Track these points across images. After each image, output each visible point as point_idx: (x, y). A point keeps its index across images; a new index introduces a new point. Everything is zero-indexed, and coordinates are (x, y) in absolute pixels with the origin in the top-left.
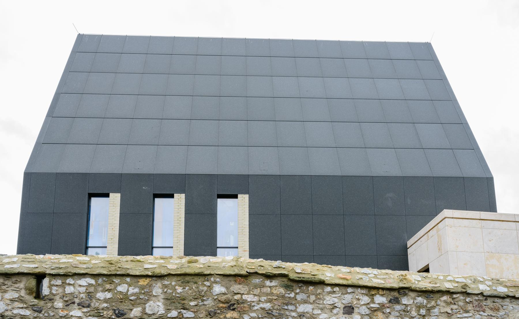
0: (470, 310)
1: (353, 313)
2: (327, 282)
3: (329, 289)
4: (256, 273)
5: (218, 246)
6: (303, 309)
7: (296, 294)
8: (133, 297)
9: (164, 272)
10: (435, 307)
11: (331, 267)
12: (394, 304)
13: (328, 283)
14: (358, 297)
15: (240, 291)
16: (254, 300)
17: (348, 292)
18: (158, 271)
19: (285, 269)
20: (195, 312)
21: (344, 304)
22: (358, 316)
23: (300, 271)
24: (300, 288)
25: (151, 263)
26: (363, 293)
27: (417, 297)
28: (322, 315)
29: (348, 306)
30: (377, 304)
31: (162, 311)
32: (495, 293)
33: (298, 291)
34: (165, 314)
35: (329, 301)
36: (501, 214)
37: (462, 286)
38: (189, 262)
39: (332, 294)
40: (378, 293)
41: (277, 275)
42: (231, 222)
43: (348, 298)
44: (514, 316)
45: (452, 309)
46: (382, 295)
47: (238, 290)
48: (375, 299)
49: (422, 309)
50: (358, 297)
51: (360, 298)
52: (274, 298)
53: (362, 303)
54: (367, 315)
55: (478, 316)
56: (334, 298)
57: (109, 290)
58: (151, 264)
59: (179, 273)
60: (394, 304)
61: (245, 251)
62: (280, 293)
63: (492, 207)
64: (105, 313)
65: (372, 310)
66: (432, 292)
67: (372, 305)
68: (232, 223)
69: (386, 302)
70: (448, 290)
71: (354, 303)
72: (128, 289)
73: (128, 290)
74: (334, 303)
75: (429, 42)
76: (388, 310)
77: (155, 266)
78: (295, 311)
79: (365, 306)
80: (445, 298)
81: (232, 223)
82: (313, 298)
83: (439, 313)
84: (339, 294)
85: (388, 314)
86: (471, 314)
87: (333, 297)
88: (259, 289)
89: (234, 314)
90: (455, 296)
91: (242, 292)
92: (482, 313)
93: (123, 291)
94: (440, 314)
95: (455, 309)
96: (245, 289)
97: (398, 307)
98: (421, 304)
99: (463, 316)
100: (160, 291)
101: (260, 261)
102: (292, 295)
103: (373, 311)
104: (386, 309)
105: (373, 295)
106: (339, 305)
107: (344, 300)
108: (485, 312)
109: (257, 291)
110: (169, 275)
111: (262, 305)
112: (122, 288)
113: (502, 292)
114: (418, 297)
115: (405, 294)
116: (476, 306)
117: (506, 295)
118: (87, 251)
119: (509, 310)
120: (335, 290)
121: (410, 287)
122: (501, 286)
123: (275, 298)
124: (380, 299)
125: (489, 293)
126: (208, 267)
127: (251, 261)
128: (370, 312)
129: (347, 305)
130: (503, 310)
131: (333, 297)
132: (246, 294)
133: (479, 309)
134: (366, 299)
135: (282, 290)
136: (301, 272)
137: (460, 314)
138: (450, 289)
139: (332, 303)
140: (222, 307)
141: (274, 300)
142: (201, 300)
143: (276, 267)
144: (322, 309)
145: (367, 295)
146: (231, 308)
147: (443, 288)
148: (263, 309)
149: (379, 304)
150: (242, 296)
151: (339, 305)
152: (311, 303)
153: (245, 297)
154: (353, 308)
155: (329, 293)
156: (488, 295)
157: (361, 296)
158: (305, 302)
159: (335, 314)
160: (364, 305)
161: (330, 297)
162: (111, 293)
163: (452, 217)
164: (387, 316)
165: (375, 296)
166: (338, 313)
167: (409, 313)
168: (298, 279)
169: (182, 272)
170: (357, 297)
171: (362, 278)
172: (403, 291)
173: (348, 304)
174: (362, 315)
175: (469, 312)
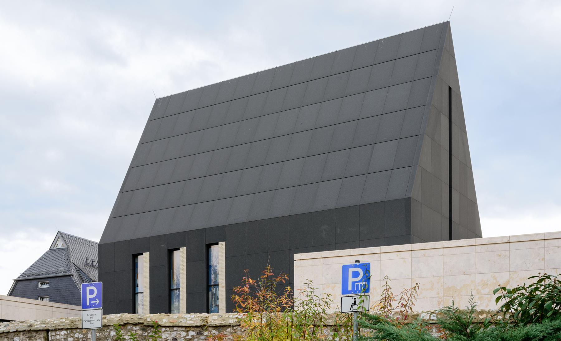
3: (164, 329)
46: (193, 331)
53: (182, 336)
61: (223, 287)
67: (187, 337)
71: (178, 337)
73: (79, 336)
75: (447, 20)
80: (229, 330)
90: (235, 328)
102: (146, 334)
105: (188, 331)
114: (213, 330)
145: (185, 331)
149: (191, 336)
154: (177, 340)
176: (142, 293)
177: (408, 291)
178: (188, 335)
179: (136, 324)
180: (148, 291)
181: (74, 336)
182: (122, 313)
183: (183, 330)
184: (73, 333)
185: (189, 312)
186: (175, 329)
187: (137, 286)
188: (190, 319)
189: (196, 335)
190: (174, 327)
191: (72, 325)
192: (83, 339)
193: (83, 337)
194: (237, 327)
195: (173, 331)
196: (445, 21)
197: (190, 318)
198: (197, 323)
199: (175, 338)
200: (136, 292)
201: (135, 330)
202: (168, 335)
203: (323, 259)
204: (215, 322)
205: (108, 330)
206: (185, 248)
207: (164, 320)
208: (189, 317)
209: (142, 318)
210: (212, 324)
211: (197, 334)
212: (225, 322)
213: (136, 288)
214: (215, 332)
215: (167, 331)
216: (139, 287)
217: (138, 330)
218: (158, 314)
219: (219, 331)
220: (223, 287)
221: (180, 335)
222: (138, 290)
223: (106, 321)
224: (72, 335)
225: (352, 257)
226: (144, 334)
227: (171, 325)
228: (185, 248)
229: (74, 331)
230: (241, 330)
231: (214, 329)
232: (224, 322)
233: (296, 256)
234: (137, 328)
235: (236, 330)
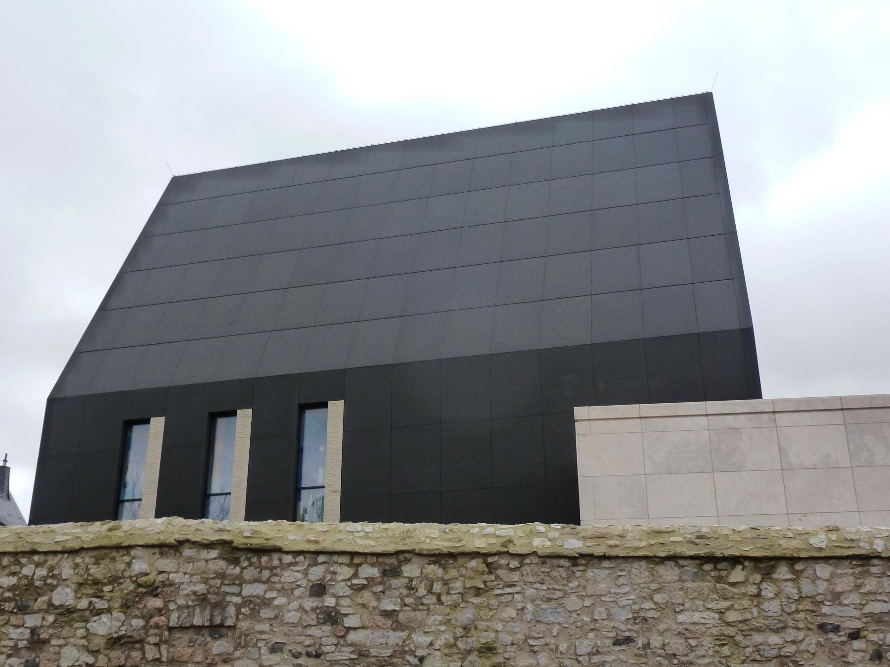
0: (517, 582)
1: (326, 594)
2: (286, 549)
3: (288, 559)
4: (188, 541)
5: (303, 486)
6: (251, 591)
7: (243, 568)
8: (38, 582)
9: (76, 545)
10: (457, 578)
11: (303, 526)
12: (390, 578)
13: (287, 550)
14: (334, 570)
15: (166, 568)
16: (184, 580)
17: (319, 562)
18: (69, 546)
19: (230, 533)
20: (110, 600)
21: (312, 581)
22: (332, 599)
23: (249, 535)
24: (248, 559)
25: (65, 534)
26: (341, 562)
27: (427, 565)
28: (278, 599)
29: (317, 584)
30: (364, 578)
31: (70, 601)
32: (559, 551)
33: (245, 564)
34: (625, 582)
35: (288, 578)
36: (773, 402)
37: (502, 543)
38: (110, 530)
39: (293, 566)
40: (366, 561)
41: (215, 542)
42: (320, 447)
43: (317, 573)
44: (594, 588)
45: (485, 582)
46: (373, 565)
47: (164, 567)
48: (359, 571)
49: (436, 583)
50: (333, 568)
51: (336, 570)
52: (210, 576)
53: (339, 579)
54: (346, 596)
55: (531, 590)
56: (296, 573)
57: (14, 574)
58: (66, 535)
59: (92, 546)
60: (390, 577)
61: (335, 492)
62: (220, 568)
63: (753, 390)
64: (7, 605)
65: (356, 588)
66: (452, 556)
67: (355, 581)
68: (322, 447)
69: (378, 575)
70: (477, 550)
71: (327, 579)
72: (34, 572)
73: (34, 573)
74: (296, 580)
75: (709, 91)
76: (380, 588)
77: (69, 537)
78: (239, 594)
79: (344, 583)
80: (473, 563)
81: (322, 447)
82: (266, 574)
83: (464, 589)
84: (304, 566)
85: (379, 593)
86: (518, 589)
87: (295, 571)
88: (191, 564)
89: (156, 602)
90: (490, 560)
91: (168, 570)
92: (538, 586)
93: (29, 574)
94: (466, 590)
95: (491, 581)
96: (172, 565)
97: (395, 582)
98: (435, 575)
99: (505, 593)
100: (71, 571)
101: (200, 523)
102: (237, 570)
103: (356, 589)
104: (378, 586)
105: (359, 565)
106: (304, 583)
107: (312, 574)
108: (544, 584)
109: (189, 568)
110: (82, 549)
111: (193, 588)
112: (27, 570)
113: (572, 549)
114: (429, 564)
115: (408, 561)
116: (527, 574)
117: (577, 553)
118: (120, 508)
119: (585, 578)
120: (298, 559)
121: (414, 549)
122: (573, 539)
123: (212, 577)
124: (369, 571)
125: (548, 552)
126: (129, 536)
127: (187, 524)
128: (352, 591)
129: (316, 582)
130: (576, 579)
131: (295, 571)
132: (174, 572)
133: (534, 579)
134: (347, 572)
135: (222, 564)
136: (250, 535)
137: (500, 589)
138: (481, 550)
139: (293, 580)
140: (141, 593)
141: (210, 579)
142: (118, 583)
143: (218, 531)
144: (279, 591)
145: (348, 566)
146: (154, 594)
147: (469, 548)
148: (195, 593)
149: (366, 579)
150: (169, 575)
151: (304, 583)
152: (264, 583)
153: (172, 576)
154: (325, 587)
155: (290, 564)
156: (546, 554)
157: (339, 567)
158: (257, 580)
159: (297, 597)
160: (344, 580)
161: (289, 572)
162: (15, 577)
163: (591, 422)
164: (378, 597)
165: (361, 566)
166: (302, 595)
167: (415, 590)
168: (242, 546)
169: (97, 545)
170: (332, 569)
171: (341, 540)
172: (403, 556)
173: (317, 581)
174: (339, 597)
175: (515, 585)
176: (140, 500)
177: (649, 535)
178: (355, 575)
179: (210, 546)
180: (154, 497)
181: (20, 572)
182: (169, 516)
183: (344, 561)
184: (19, 563)
185: (344, 518)
186: (321, 559)
187: (125, 487)
188: (364, 534)
189: (380, 577)
190: (317, 553)
191: (20, 543)
192: (45, 581)
193: (47, 577)
194: (496, 558)
195: (315, 565)
196: (705, 92)
197: (363, 534)
198: (385, 545)
199: (319, 582)
200: (121, 499)
201: (207, 561)
202: (299, 575)
203: (643, 420)
204: (435, 542)
205: (127, 559)
206: (249, 412)
207: (291, 537)
208: (360, 529)
209: (228, 528)
210: (429, 547)
211: (384, 573)
212: (463, 543)
213: (122, 490)
214: (433, 570)
215: (298, 562)
216: (127, 489)
217: (215, 559)
218: (270, 521)
219: (444, 567)
220: (335, 492)
221: (333, 576)
222: (124, 496)
223: (122, 534)
224: (14, 568)
225: (710, 417)
226: (229, 571)
227: (312, 548)
228: (249, 412)
229: (24, 560)
230: (508, 564)
231: (434, 563)
232: (460, 544)
233: (580, 412)
234: (214, 553)
235: (493, 566)
